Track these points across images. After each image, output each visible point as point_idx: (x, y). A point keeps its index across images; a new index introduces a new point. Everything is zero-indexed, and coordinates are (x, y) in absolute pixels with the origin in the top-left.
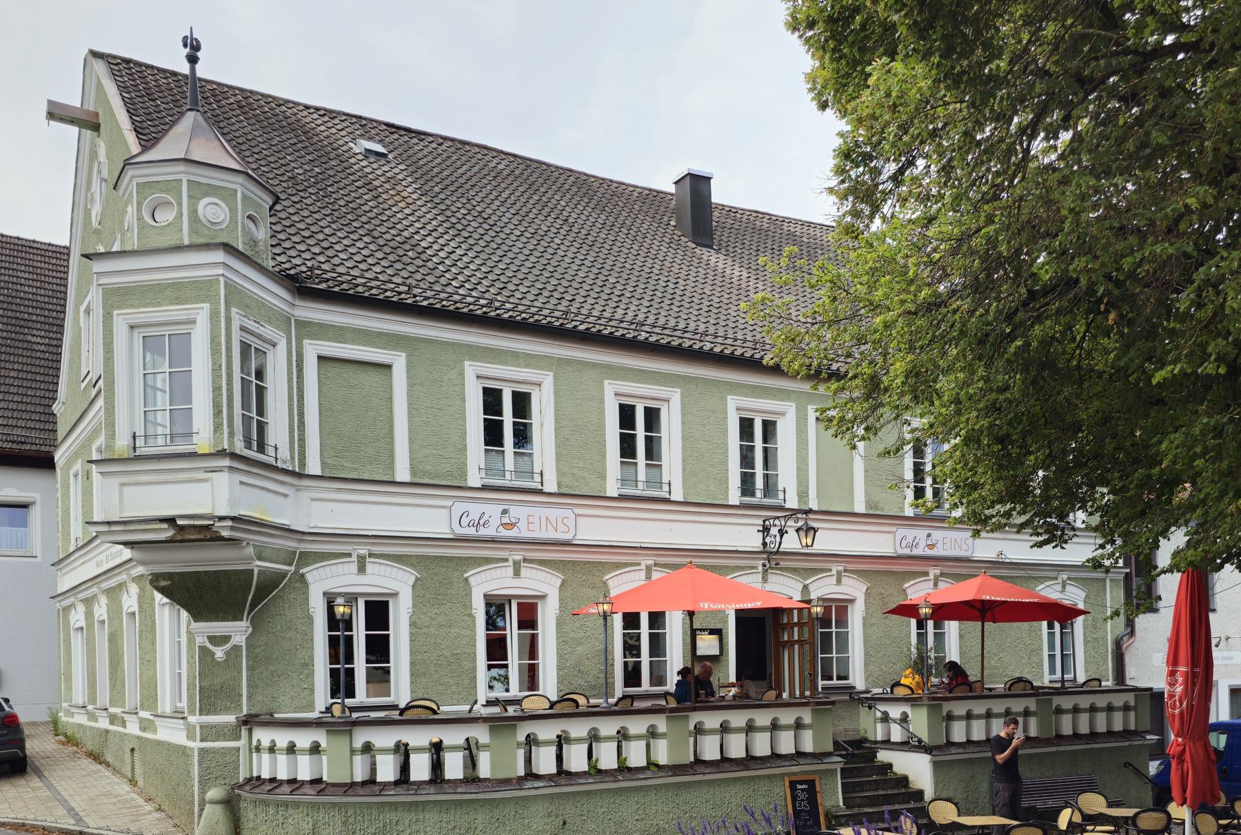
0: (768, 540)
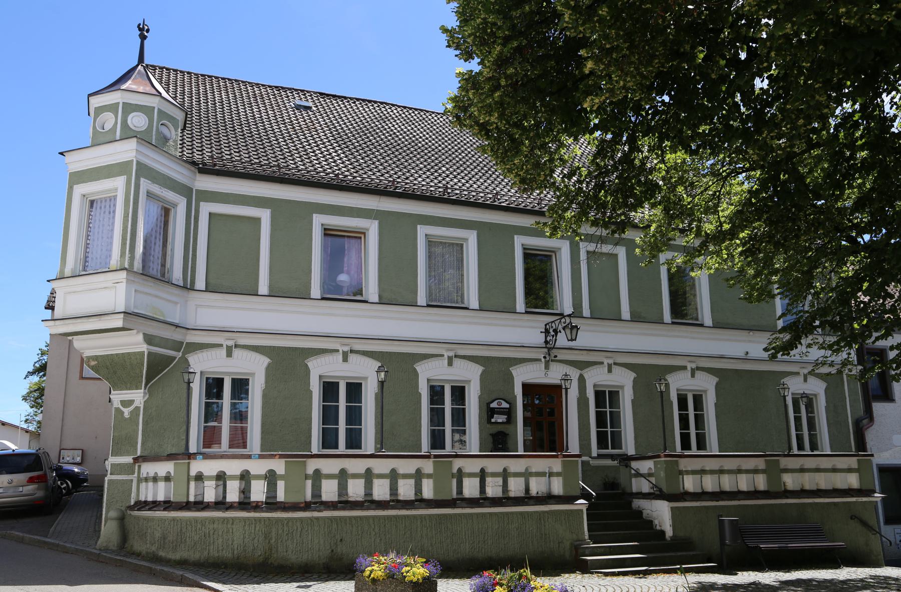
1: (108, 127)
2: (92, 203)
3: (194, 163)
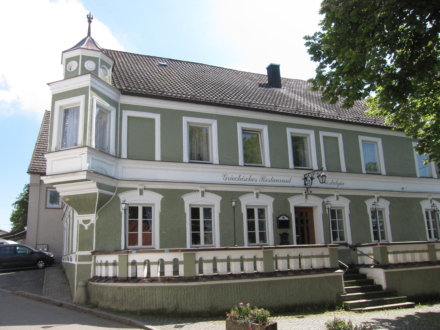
0: (307, 182)
1: (73, 69)
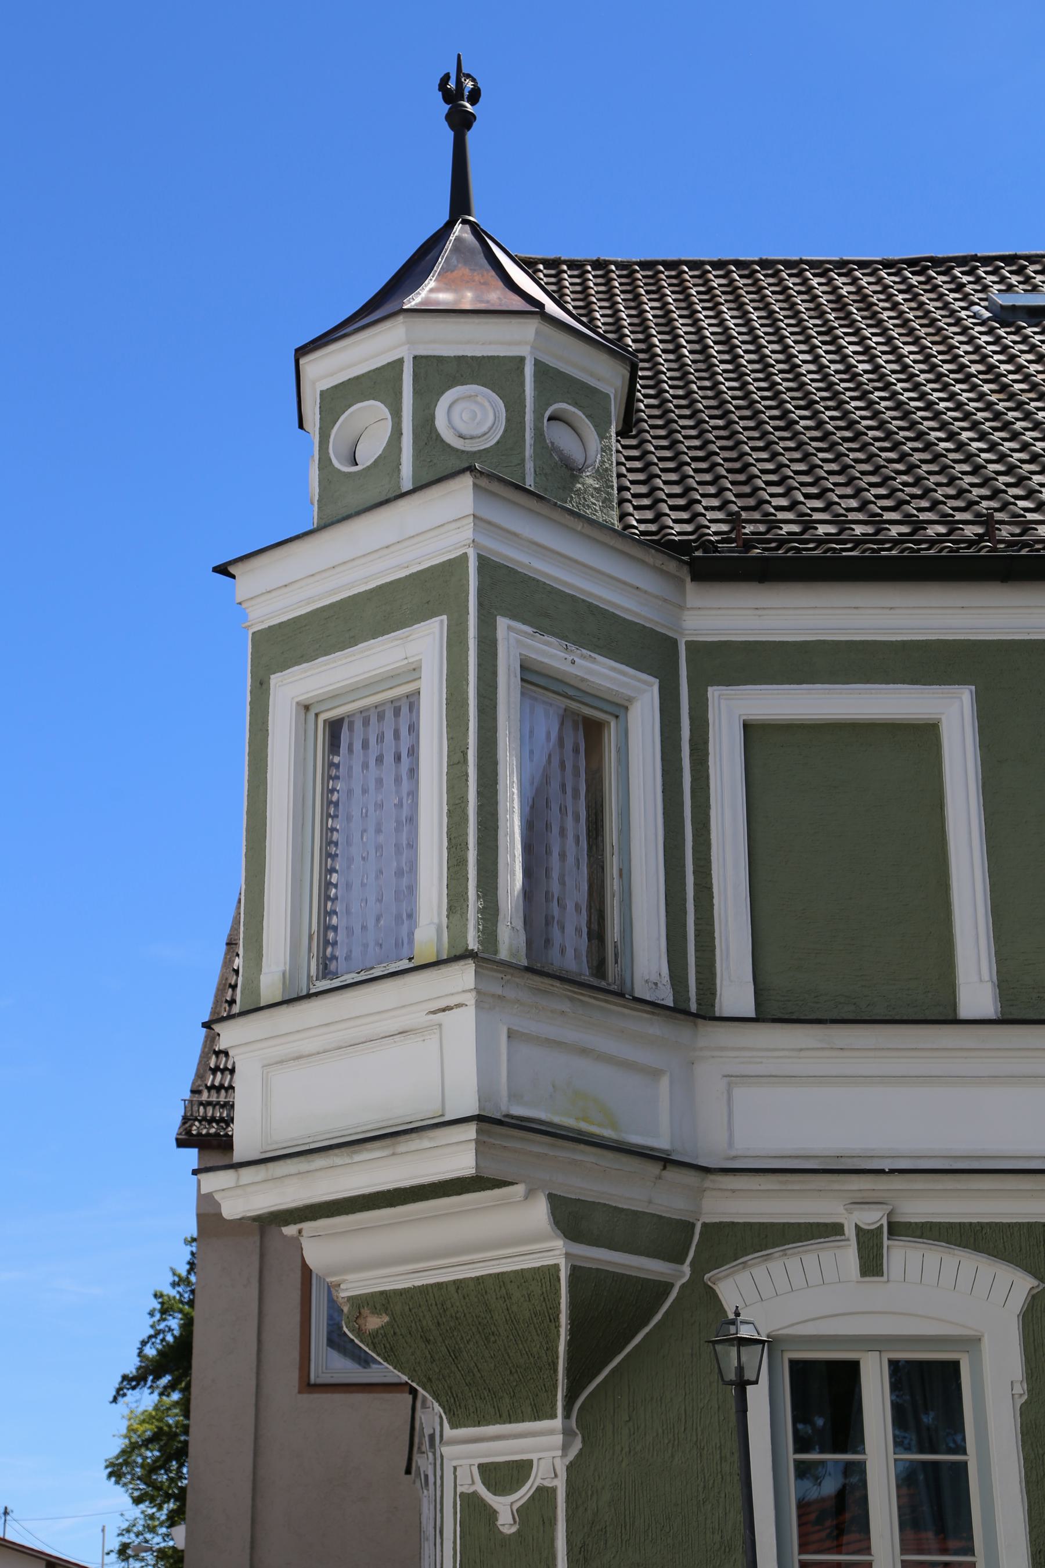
1: (369, 451)
2: (335, 728)
3: (663, 545)
